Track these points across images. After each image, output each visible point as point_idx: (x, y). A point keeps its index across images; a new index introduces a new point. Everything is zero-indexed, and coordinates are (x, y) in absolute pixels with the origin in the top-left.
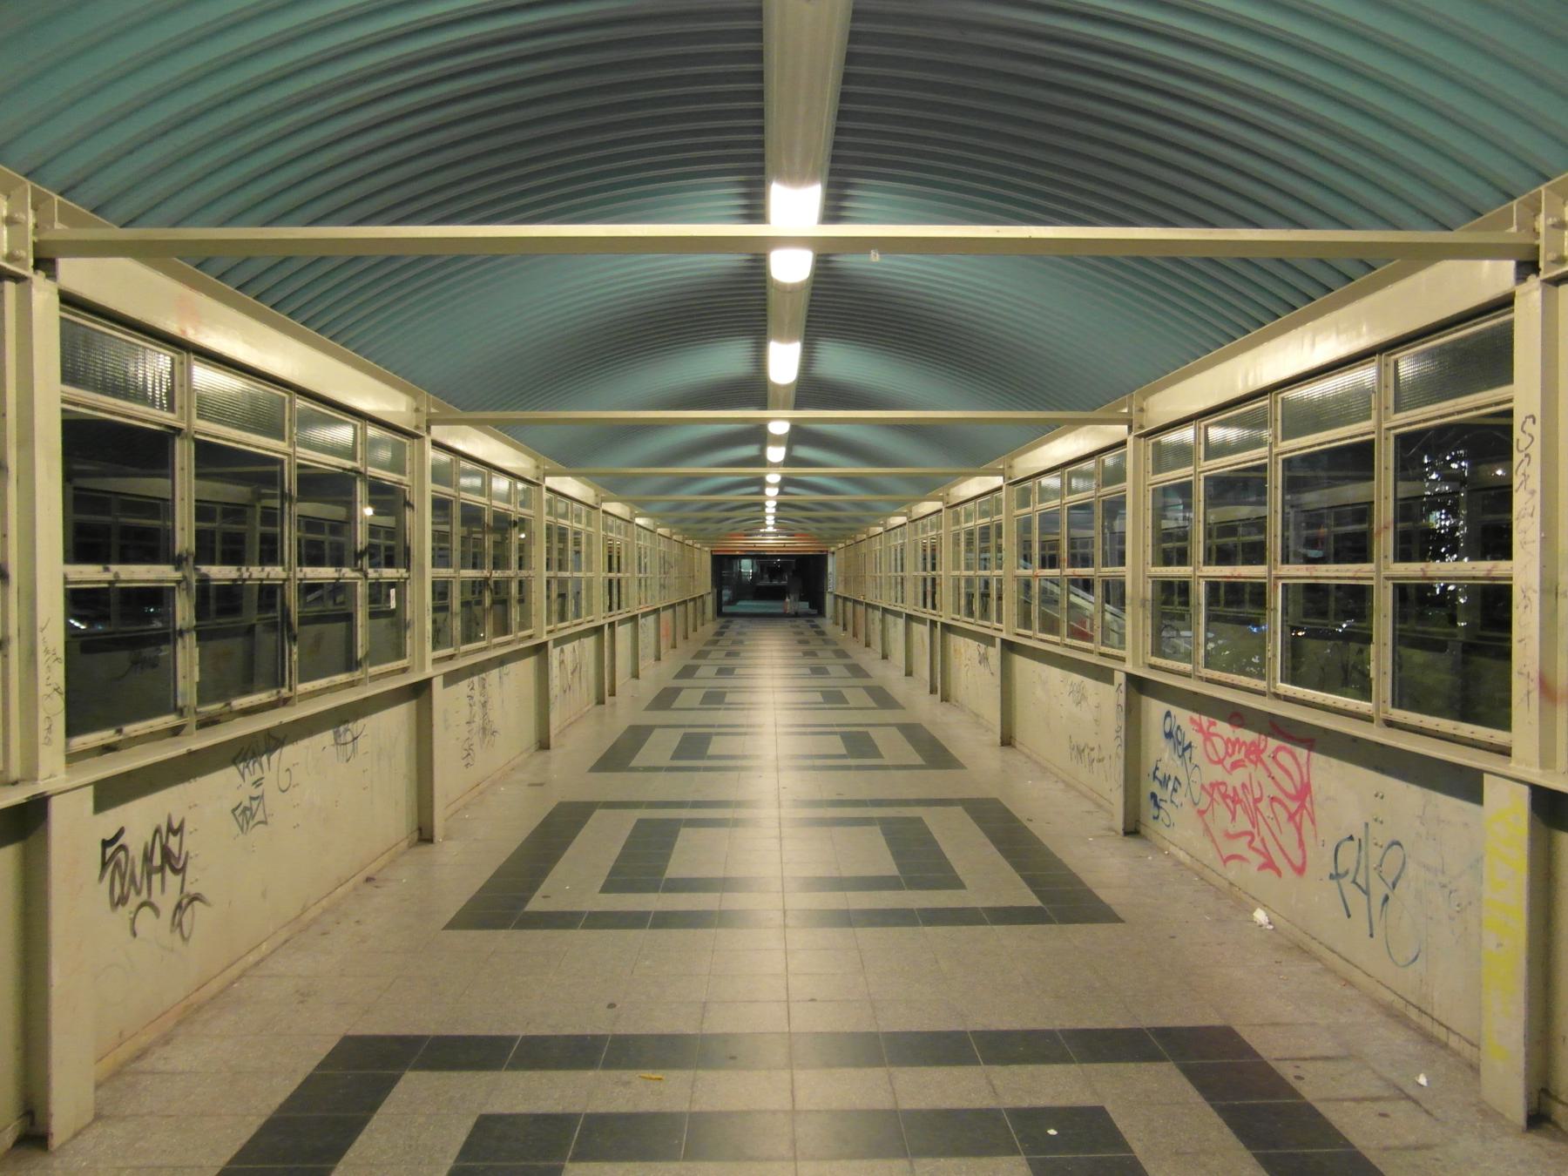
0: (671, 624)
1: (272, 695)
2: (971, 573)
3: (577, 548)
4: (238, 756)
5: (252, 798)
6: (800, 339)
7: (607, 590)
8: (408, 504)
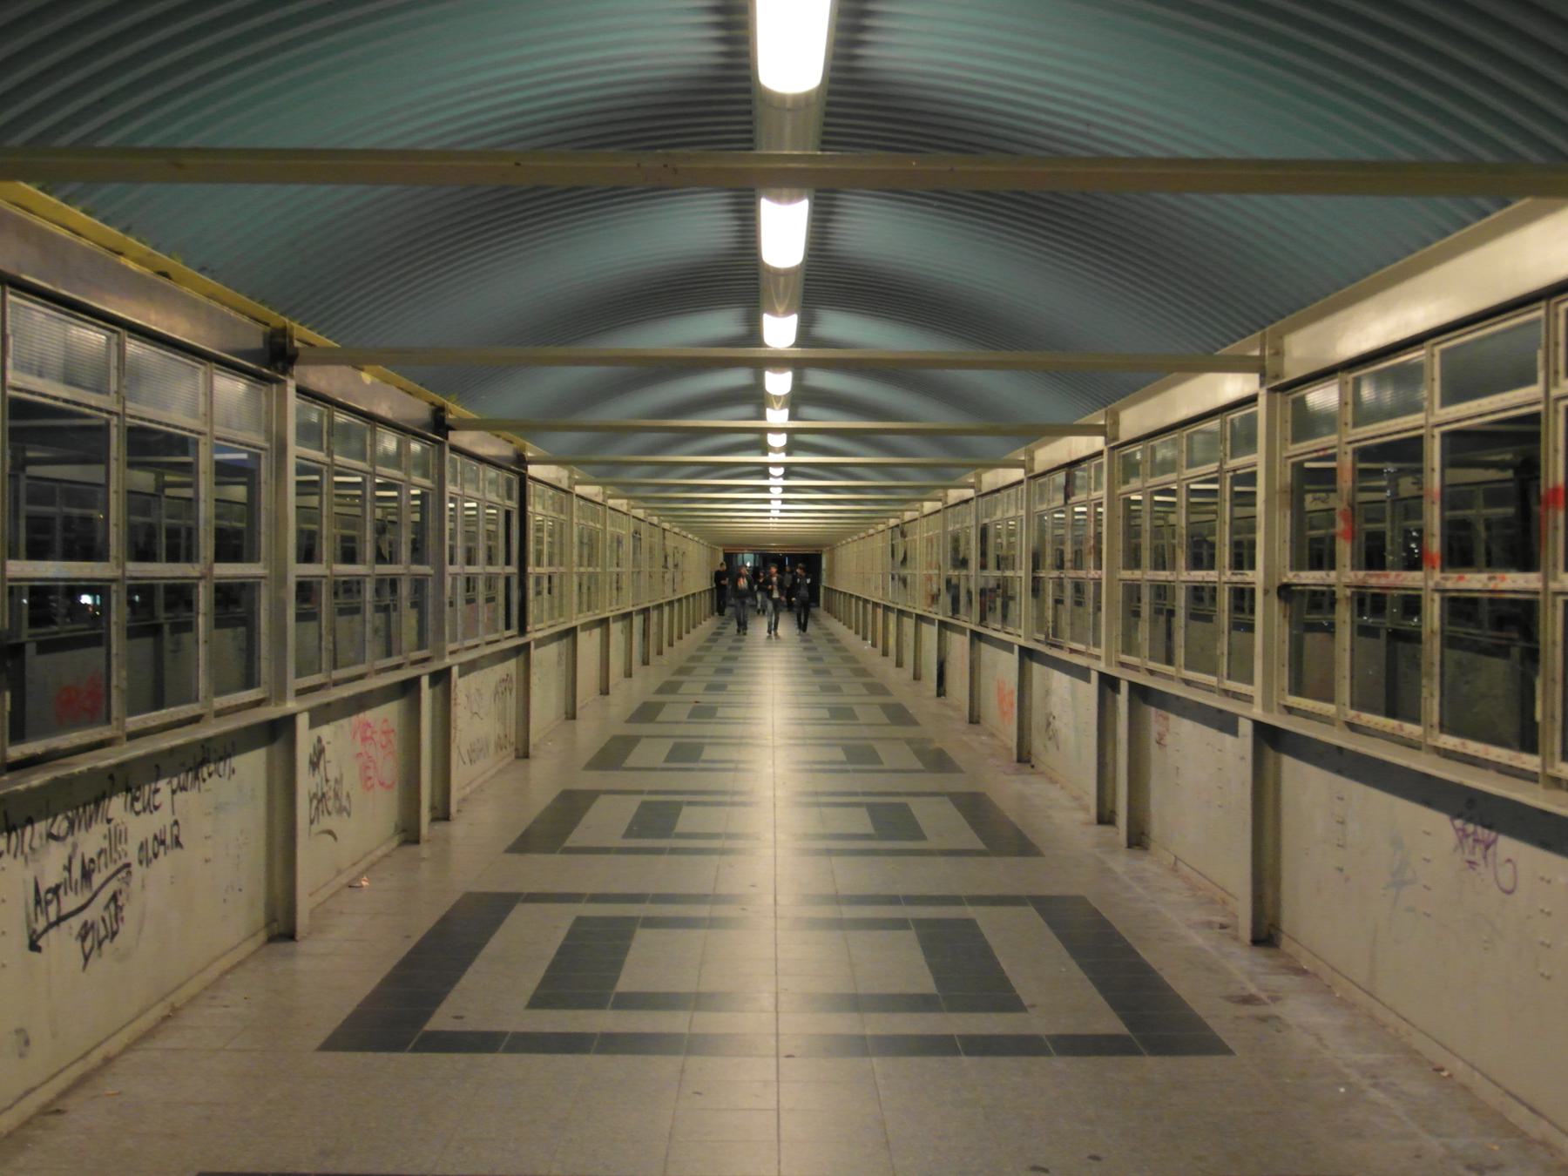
6: (796, 312)
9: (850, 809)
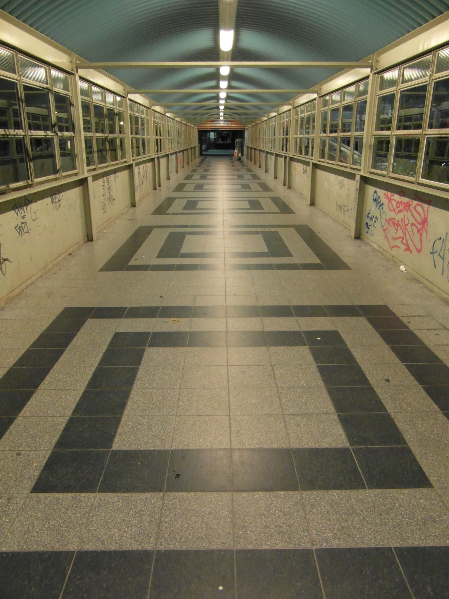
0: (182, 158)
1: (25, 183)
2: (302, 136)
3: (143, 127)
4: (15, 206)
5: (22, 223)
7: (156, 144)
8: (72, 104)
9: (248, 215)
